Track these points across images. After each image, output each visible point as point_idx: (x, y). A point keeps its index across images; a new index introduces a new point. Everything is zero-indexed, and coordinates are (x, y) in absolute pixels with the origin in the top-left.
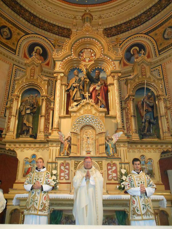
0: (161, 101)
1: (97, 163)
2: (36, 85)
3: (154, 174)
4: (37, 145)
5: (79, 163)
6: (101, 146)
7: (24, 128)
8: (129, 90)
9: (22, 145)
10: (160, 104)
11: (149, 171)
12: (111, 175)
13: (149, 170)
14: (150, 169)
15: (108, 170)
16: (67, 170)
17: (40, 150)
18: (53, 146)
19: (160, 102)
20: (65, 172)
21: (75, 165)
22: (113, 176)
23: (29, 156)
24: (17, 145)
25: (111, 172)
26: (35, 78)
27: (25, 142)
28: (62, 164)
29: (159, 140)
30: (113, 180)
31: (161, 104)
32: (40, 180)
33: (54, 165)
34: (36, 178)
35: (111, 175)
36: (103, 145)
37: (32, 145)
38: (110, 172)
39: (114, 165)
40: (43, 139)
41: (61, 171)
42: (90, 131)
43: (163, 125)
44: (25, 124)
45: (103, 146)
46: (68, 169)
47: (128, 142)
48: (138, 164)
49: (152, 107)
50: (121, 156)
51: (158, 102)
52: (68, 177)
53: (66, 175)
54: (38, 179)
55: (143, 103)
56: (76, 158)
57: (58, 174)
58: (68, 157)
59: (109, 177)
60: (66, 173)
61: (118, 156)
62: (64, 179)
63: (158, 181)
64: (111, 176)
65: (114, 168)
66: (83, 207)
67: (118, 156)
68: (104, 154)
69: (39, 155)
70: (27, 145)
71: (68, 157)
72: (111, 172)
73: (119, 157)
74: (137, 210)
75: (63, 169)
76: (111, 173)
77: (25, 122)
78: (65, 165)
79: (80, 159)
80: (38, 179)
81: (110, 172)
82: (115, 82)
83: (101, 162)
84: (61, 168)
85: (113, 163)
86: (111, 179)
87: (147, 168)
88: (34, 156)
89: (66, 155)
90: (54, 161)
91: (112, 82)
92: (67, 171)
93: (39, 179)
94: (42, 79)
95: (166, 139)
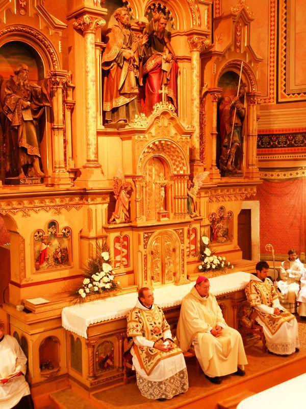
0: (253, 106)
2: (40, 42)
4: (58, 201)
7: (23, 160)
8: (214, 69)
9: (26, 203)
10: (251, 110)
16: (125, 249)
17: (63, 210)
18: (97, 204)
19: (251, 107)
20: (123, 252)
23: (43, 225)
24: (15, 204)
26: (31, 13)
27: (31, 197)
28: (117, 240)
31: (253, 111)
32: (159, 323)
33: (100, 242)
34: (151, 322)
37: (47, 202)
40: (68, 187)
41: (117, 252)
42: (149, 65)
43: (250, 152)
44: (25, 150)
46: (127, 247)
48: (149, 386)
51: (248, 106)
52: (128, 262)
53: (124, 259)
54: (155, 323)
55: (233, 107)
57: (113, 259)
62: (122, 267)
69: (63, 223)
70: (37, 202)
74: (150, 351)
75: (119, 248)
77: (24, 143)
78: (122, 240)
80: (155, 323)
82: (196, 56)
84: (25, 120)
88: (53, 224)
90: (100, 234)
91: (187, 54)
92: (125, 251)
93: (157, 322)
94: (50, 21)
95: (253, 173)
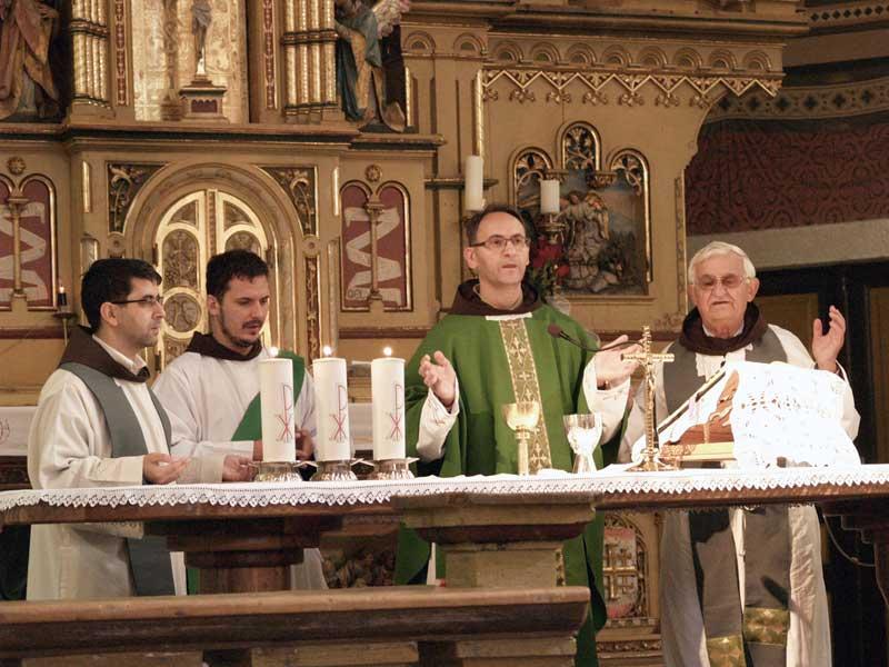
1: (278, 178)
3: (649, 266)
5: (144, 178)
6: (297, 44)
11: (614, 242)
12: (361, 268)
13: (611, 233)
14: (617, 231)
15: (350, 231)
21: (112, 198)
22: (382, 278)
25: (368, 249)
29: (710, 14)
30: (377, 306)
35: (361, 268)
36: (322, 42)
38: (356, 250)
39: (394, 194)
45: (316, 50)
47: (490, 21)
49: (476, 297)
50: (434, 131)
53: (31, 276)
56: (254, 144)
58: (46, 128)
59: (352, 285)
60: (28, 257)
61: (414, 130)
63: (667, 317)
64: (361, 278)
65: (388, 221)
66: (380, 293)
67: (414, 130)
68: (327, 113)
71: (46, 128)
72: (368, 249)
73: (424, 134)
76: (363, 259)
79: (314, 153)
81: (356, 250)
83: (302, 178)
85: (381, 181)
86: (367, 303)
87: (604, 219)
89: (32, 109)
